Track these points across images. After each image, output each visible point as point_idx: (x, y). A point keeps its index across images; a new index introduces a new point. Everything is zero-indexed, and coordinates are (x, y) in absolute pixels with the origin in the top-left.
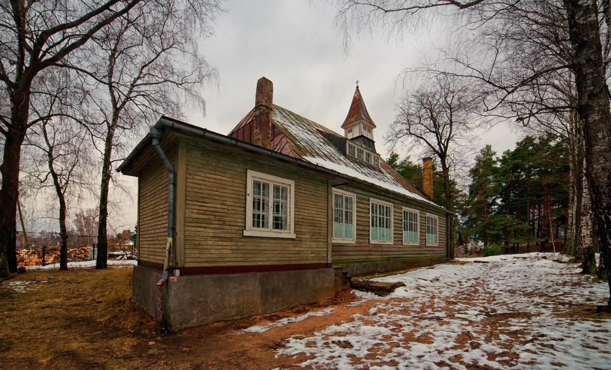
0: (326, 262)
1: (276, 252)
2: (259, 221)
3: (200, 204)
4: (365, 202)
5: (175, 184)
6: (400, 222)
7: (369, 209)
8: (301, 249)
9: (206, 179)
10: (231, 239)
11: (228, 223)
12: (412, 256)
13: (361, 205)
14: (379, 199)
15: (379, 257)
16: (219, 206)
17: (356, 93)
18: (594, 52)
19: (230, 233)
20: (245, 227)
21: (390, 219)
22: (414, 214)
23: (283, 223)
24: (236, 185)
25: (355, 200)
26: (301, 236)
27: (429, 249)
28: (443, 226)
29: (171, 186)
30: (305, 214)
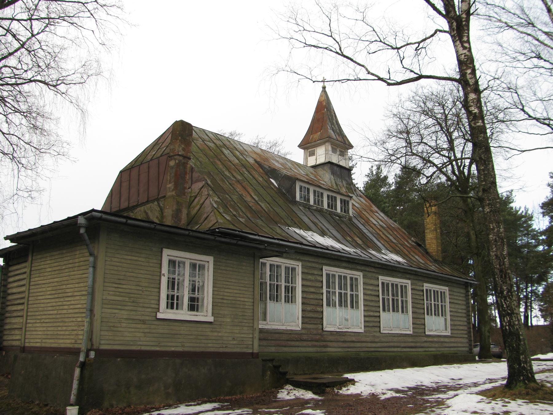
0: (251, 351)
1: (191, 337)
2: (173, 302)
3: (116, 286)
4: (316, 273)
5: (94, 267)
7: (322, 282)
8: (220, 334)
9: (123, 261)
10: (144, 322)
11: (142, 304)
12: (399, 349)
13: (310, 277)
15: (340, 350)
16: (133, 287)
17: (321, 96)
18: (483, 152)
19: (143, 315)
20: (159, 309)
23: (200, 304)
24: (151, 265)
25: (299, 270)
26: (220, 319)
27: (430, 339)
28: (460, 302)
29: (91, 270)
30: (226, 294)
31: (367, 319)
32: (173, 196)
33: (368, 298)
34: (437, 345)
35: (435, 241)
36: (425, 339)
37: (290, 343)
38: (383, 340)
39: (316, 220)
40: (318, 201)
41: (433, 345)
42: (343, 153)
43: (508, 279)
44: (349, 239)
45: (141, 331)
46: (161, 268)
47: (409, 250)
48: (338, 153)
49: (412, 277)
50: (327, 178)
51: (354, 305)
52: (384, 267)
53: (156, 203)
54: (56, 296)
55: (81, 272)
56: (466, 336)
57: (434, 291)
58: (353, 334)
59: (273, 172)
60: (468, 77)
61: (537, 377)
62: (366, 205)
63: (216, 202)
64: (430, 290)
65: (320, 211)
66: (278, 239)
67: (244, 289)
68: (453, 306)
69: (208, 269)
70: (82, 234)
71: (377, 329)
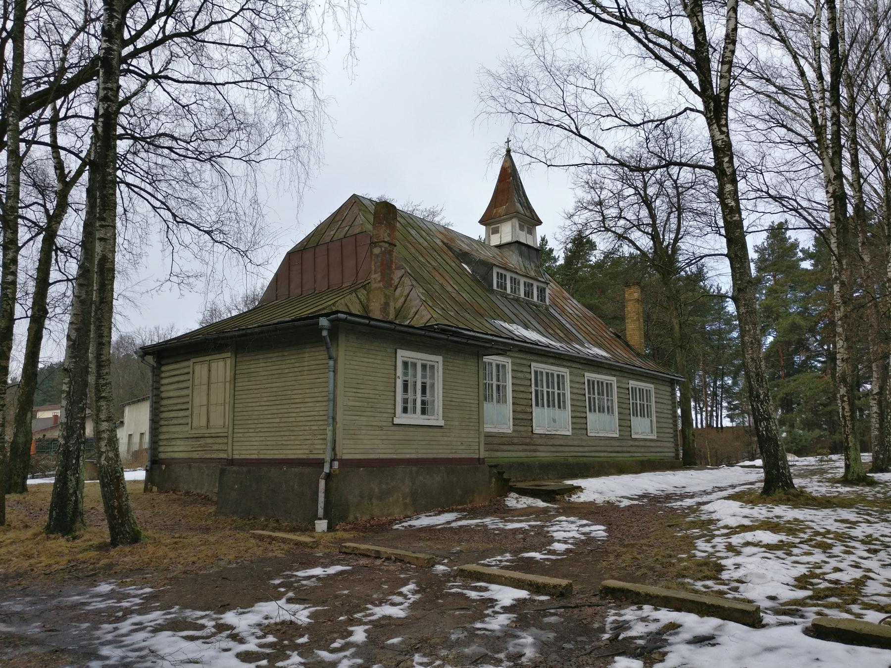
0: (477, 457)
5: (335, 372)
6: (582, 398)
7: (531, 380)
8: (450, 439)
9: (361, 364)
10: (381, 428)
12: (606, 454)
13: (519, 375)
14: (546, 363)
15: (548, 454)
16: (371, 392)
17: (505, 161)
20: (395, 413)
21: (564, 394)
22: (607, 384)
25: (509, 367)
27: (637, 443)
28: (665, 401)
29: (332, 374)
30: (454, 396)
31: (574, 420)
32: (380, 288)
33: (574, 397)
34: (643, 450)
35: (637, 333)
36: (631, 443)
37: (501, 447)
38: (590, 444)
39: (515, 311)
40: (515, 289)
41: (639, 450)
42: (531, 231)
43: (764, 383)
44: (551, 331)
45: (379, 437)
46: (395, 370)
47: (610, 342)
48: (526, 229)
49: (617, 373)
50: (514, 259)
51: (610, 410)
52: (589, 363)
53: (354, 294)
54: (277, 402)
55: (314, 377)
56: (672, 440)
57: (639, 389)
58: (561, 437)
59: (464, 257)
60: (726, 165)
61: (797, 482)
62: (557, 291)
63: (422, 294)
64: (636, 388)
65: (517, 300)
66: (491, 335)
67: (470, 389)
68: (659, 405)
69: (438, 369)
70: (324, 337)
71: (584, 432)
